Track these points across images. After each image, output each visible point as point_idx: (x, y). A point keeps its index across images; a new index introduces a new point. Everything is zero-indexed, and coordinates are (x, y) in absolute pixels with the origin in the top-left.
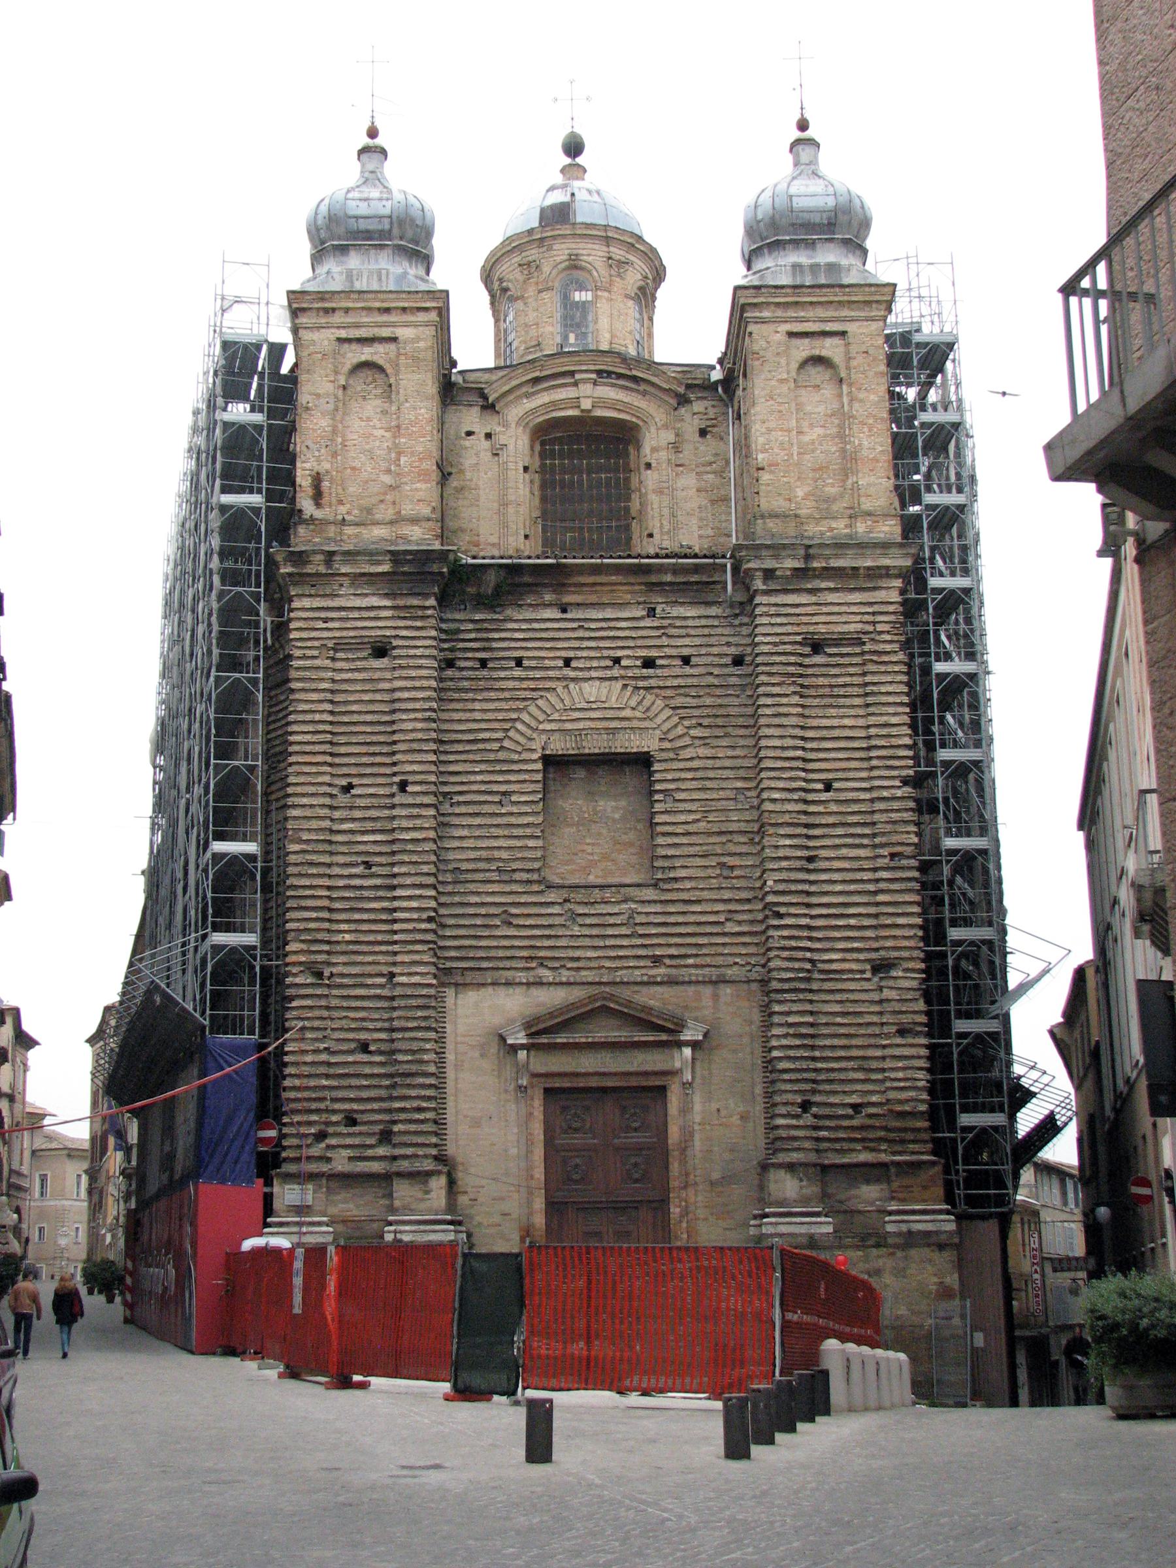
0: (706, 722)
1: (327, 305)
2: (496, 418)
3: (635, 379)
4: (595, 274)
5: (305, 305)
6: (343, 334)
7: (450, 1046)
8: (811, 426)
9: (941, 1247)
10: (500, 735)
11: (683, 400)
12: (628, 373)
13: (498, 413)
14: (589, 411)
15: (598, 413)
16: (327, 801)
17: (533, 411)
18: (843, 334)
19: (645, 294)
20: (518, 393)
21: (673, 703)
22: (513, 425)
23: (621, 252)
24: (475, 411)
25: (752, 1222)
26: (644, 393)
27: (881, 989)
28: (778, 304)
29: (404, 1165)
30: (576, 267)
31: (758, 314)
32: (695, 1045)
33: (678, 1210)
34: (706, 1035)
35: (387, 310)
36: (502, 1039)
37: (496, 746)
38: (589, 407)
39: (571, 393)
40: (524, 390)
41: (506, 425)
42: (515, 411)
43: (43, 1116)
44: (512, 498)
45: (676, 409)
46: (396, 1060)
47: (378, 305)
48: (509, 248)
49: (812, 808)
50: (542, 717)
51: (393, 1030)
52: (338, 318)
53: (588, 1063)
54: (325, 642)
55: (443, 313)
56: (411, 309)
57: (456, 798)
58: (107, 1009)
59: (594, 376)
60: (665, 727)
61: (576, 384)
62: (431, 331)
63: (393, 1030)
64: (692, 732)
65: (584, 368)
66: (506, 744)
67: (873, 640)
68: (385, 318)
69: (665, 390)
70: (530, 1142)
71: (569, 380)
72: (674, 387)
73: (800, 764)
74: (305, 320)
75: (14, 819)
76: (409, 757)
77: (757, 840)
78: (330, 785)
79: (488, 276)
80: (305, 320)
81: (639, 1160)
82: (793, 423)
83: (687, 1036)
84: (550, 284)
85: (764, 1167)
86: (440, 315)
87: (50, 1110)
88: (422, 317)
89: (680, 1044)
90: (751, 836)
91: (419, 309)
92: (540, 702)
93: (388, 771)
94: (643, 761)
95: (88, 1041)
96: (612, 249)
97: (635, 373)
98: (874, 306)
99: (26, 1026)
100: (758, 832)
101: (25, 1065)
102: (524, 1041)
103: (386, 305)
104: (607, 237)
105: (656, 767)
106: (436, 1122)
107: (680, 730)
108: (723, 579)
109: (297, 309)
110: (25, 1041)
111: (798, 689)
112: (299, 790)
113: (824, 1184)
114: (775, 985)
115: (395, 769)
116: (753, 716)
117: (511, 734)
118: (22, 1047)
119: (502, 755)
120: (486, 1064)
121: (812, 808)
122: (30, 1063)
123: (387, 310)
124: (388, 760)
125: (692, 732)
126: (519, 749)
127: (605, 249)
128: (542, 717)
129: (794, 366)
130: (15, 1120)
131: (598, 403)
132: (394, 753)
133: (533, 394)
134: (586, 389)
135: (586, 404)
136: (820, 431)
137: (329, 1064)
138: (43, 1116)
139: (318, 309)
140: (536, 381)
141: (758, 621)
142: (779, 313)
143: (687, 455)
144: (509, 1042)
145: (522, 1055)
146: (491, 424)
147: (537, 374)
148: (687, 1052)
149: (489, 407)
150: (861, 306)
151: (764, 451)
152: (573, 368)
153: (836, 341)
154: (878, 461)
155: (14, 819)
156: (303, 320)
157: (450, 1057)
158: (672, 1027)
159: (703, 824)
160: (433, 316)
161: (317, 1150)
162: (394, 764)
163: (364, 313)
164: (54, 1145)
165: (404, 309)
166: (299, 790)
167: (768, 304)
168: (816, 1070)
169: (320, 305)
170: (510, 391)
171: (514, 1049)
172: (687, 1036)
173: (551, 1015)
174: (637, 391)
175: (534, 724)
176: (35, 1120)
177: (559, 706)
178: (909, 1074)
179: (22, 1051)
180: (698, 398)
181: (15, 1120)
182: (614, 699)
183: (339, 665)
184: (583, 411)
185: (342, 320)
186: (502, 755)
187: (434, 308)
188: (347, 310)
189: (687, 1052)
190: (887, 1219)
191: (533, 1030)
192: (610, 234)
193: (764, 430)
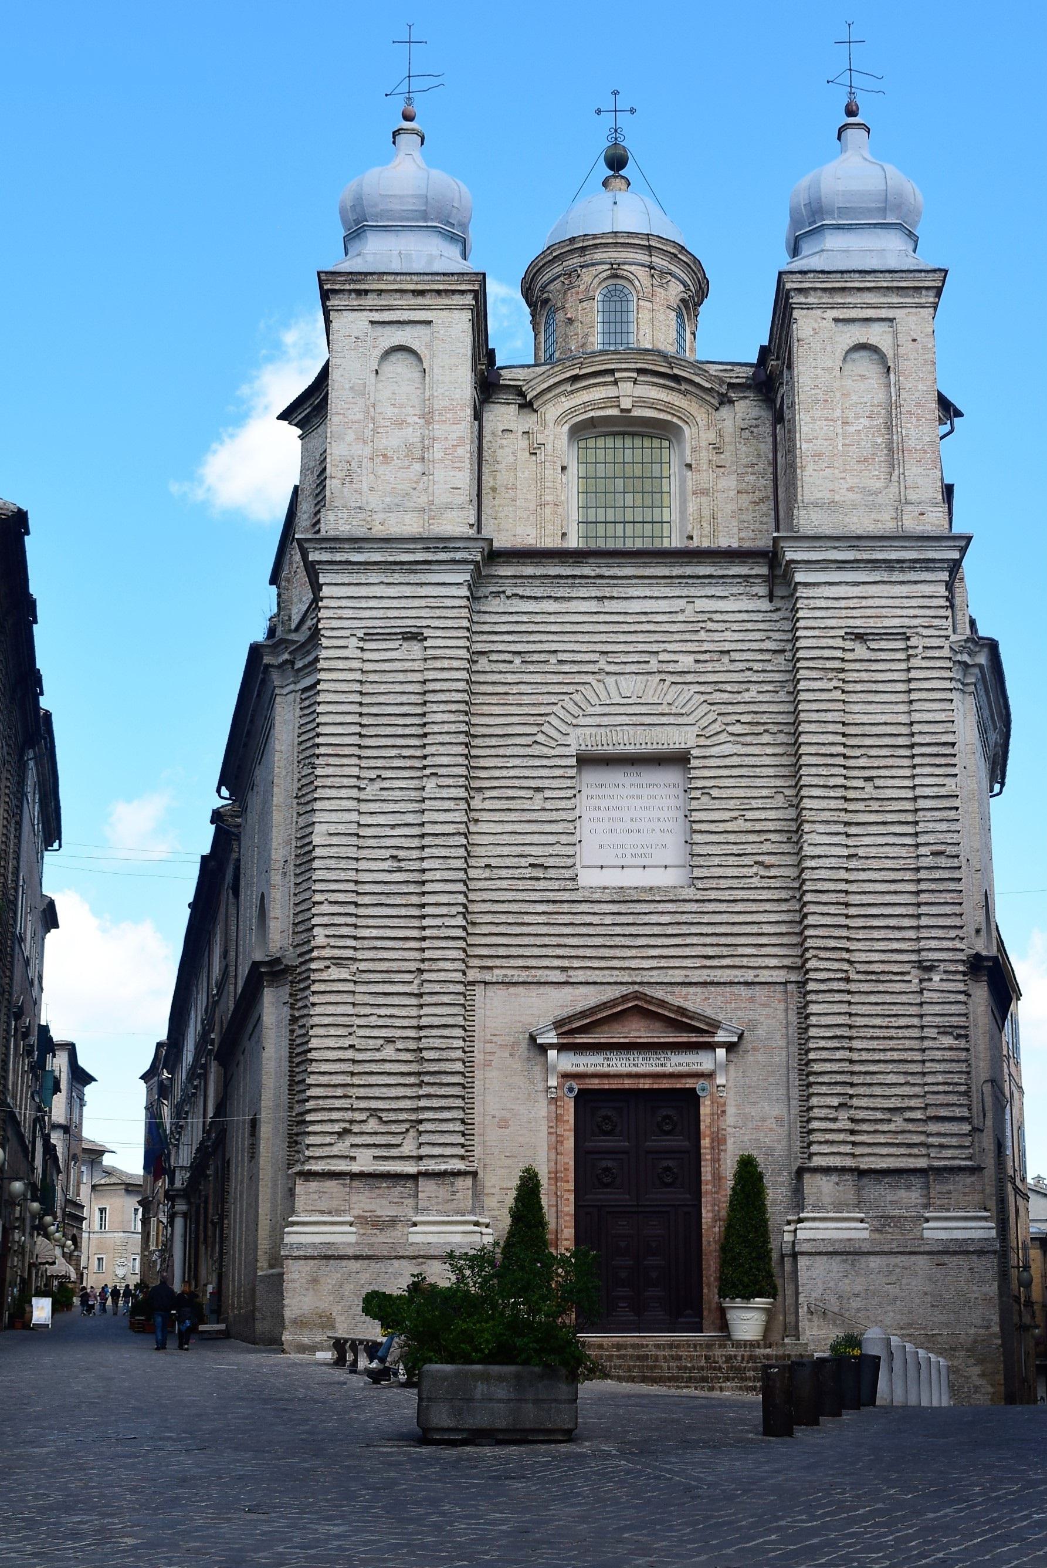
0: (744, 718)
1: (358, 287)
2: (534, 417)
3: (676, 378)
4: (637, 283)
5: (337, 287)
6: (377, 316)
7: (478, 1045)
8: (857, 417)
9: (980, 1253)
10: (534, 730)
11: (725, 401)
12: (669, 371)
13: (536, 411)
14: (629, 411)
15: (637, 413)
16: (354, 793)
17: (572, 410)
18: (891, 320)
19: (687, 307)
20: (557, 391)
21: (711, 698)
22: (551, 425)
23: (664, 263)
24: (513, 409)
25: (786, 1228)
26: (684, 393)
27: (921, 992)
28: (824, 290)
29: (432, 1166)
30: (615, 276)
31: (803, 300)
32: (730, 1047)
33: (710, 1215)
34: (741, 1036)
35: (421, 293)
36: (532, 1038)
37: (529, 740)
38: (630, 407)
39: (611, 391)
40: (562, 388)
41: (544, 425)
42: (554, 410)
43: (101, 1153)
44: (549, 498)
45: (717, 409)
46: (423, 1058)
47: (412, 287)
48: (550, 258)
49: (851, 806)
50: (575, 711)
51: (420, 1028)
52: (370, 301)
53: (620, 1064)
54: (354, 632)
55: (480, 296)
56: (446, 291)
57: (489, 794)
58: (159, 1045)
59: (635, 375)
60: (704, 722)
61: (616, 383)
62: (467, 315)
63: (420, 1028)
64: (730, 729)
65: (624, 366)
66: (540, 738)
67: (917, 634)
68: (420, 301)
69: (707, 389)
70: (559, 1141)
71: (609, 379)
72: (717, 387)
73: (840, 761)
74: (336, 303)
75: (60, 846)
76: (442, 749)
77: (795, 839)
78: (358, 777)
79: (529, 288)
80: (336, 303)
81: (670, 1163)
82: (838, 413)
83: (721, 1036)
84: (591, 294)
85: (800, 1172)
86: (476, 298)
87: (109, 1147)
88: (457, 300)
89: (711, 1047)
90: (789, 835)
91: (454, 292)
92: (577, 697)
93: (417, 764)
94: (680, 760)
95: (141, 1078)
96: (654, 259)
97: (676, 371)
98: (924, 292)
99: (82, 1062)
100: (796, 832)
101: (81, 1099)
102: (555, 1041)
103: (420, 287)
104: (650, 246)
105: (694, 763)
106: (463, 1121)
107: (716, 727)
108: (706, 1323)
109: (328, 290)
110: (81, 1077)
111: (840, 684)
112: (328, 782)
113: (859, 1189)
114: (811, 986)
115: (425, 762)
116: (794, 723)
117: (546, 728)
118: (79, 1082)
119: (536, 750)
120: (517, 1065)
121: (851, 806)
122: (86, 1098)
123: (421, 293)
124: (419, 753)
125: (730, 729)
126: (553, 744)
127: (647, 258)
128: (575, 711)
129: (840, 354)
130: (72, 1153)
131: (639, 402)
132: (424, 746)
133: (572, 392)
134: (626, 387)
135: (626, 403)
136: (865, 422)
137: (354, 1061)
138: (101, 1153)
139: (350, 291)
140: (575, 378)
141: (800, 614)
142: (826, 299)
143: (726, 457)
144: (538, 1041)
145: (552, 1054)
146: (529, 421)
147: (576, 372)
148: (721, 1052)
149: (527, 406)
150: (911, 292)
151: (810, 441)
152: (613, 366)
153: (883, 327)
154: (925, 452)
155: (60, 846)
156: (334, 302)
157: (478, 1057)
158: (706, 1028)
159: (740, 822)
160: (469, 299)
161: (342, 1147)
162: (425, 757)
163: (398, 295)
164: (113, 1180)
165: (439, 292)
166: (328, 782)
167: (815, 289)
168: (852, 1073)
169: (352, 287)
170: (549, 389)
171: (543, 1049)
172: (721, 1036)
173: (583, 1014)
174: (679, 391)
175: (569, 719)
176: (95, 1155)
177: (594, 700)
178: (949, 1078)
179: (79, 1086)
180: (741, 398)
181: (72, 1153)
182: (651, 692)
183: (367, 656)
184: (622, 410)
185: (375, 302)
186: (536, 750)
187: (470, 291)
188: (380, 292)
189: (721, 1052)
190: (926, 1225)
191: (564, 1030)
192: (653, 243)
193: (812, 375)
